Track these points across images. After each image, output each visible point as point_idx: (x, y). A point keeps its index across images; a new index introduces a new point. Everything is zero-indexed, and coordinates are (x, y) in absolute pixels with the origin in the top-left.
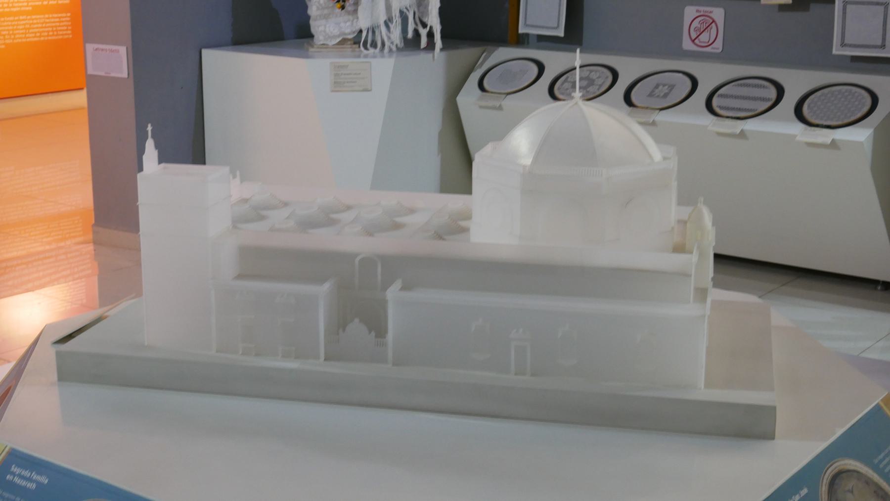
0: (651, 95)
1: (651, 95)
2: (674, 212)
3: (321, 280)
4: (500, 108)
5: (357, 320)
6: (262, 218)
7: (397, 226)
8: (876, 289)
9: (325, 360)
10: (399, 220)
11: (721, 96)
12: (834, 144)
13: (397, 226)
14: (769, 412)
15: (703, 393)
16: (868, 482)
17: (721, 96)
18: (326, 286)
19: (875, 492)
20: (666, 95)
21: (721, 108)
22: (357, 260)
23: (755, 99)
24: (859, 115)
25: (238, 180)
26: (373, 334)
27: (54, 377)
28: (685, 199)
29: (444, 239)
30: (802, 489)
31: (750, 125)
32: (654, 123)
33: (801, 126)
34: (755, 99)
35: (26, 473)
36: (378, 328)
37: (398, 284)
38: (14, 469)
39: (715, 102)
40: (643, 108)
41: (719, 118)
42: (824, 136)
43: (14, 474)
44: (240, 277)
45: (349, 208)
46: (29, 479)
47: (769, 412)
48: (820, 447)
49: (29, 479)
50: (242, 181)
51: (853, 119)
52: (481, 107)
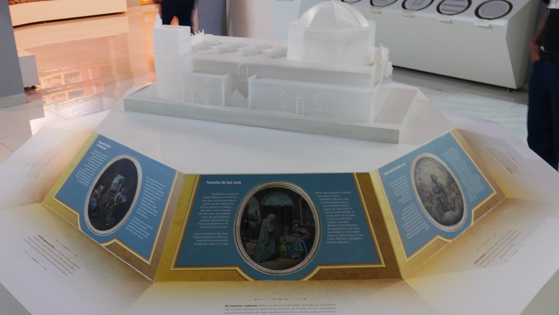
0: (414, 4)
1: (414, 4)
2: (371, 50)
3: (223, 74)
4: (380, 13)
5: (237, 90)
6: (209, 48)
7: (260, 53)
8: (506, 91)
9: (225, 106)
10: (263, 51)
11: (445, 5)
12: (490, 27)
13: (260, 53)
14: (397, 132)
15: (372, 123)
16: (436, 162)
17: (445, 5)
18: (225, 77)
19: (439, 167)
20: (420, 4)
21: (443, 10)
22: (239, 66)
23: (458, 6)
24: (503, 14)
25: (203, 33)
26: (243, 96)
27: (123, 109)
28: (377, 45)
29: (276, 58)
30: (402, 163)
31: (455, 18)
32: (413, 16)
33: (477, 18)
34: (458, 6)
35: (103, 144)
36: (245, 93)
37: (254, 76)
38: (100, 142)
39: (441, 7)
40: (409, 9)
41: (442, 15)
42: (486, 23)
43: (99, 144)
44: (195, 72)
45: (270, 47)
46: (104, 146)
47: (397, 132)
48: (415, 147)
49: (104, 146)
50: (205, 33)
51: (500, 15)
52: (372, 12)
